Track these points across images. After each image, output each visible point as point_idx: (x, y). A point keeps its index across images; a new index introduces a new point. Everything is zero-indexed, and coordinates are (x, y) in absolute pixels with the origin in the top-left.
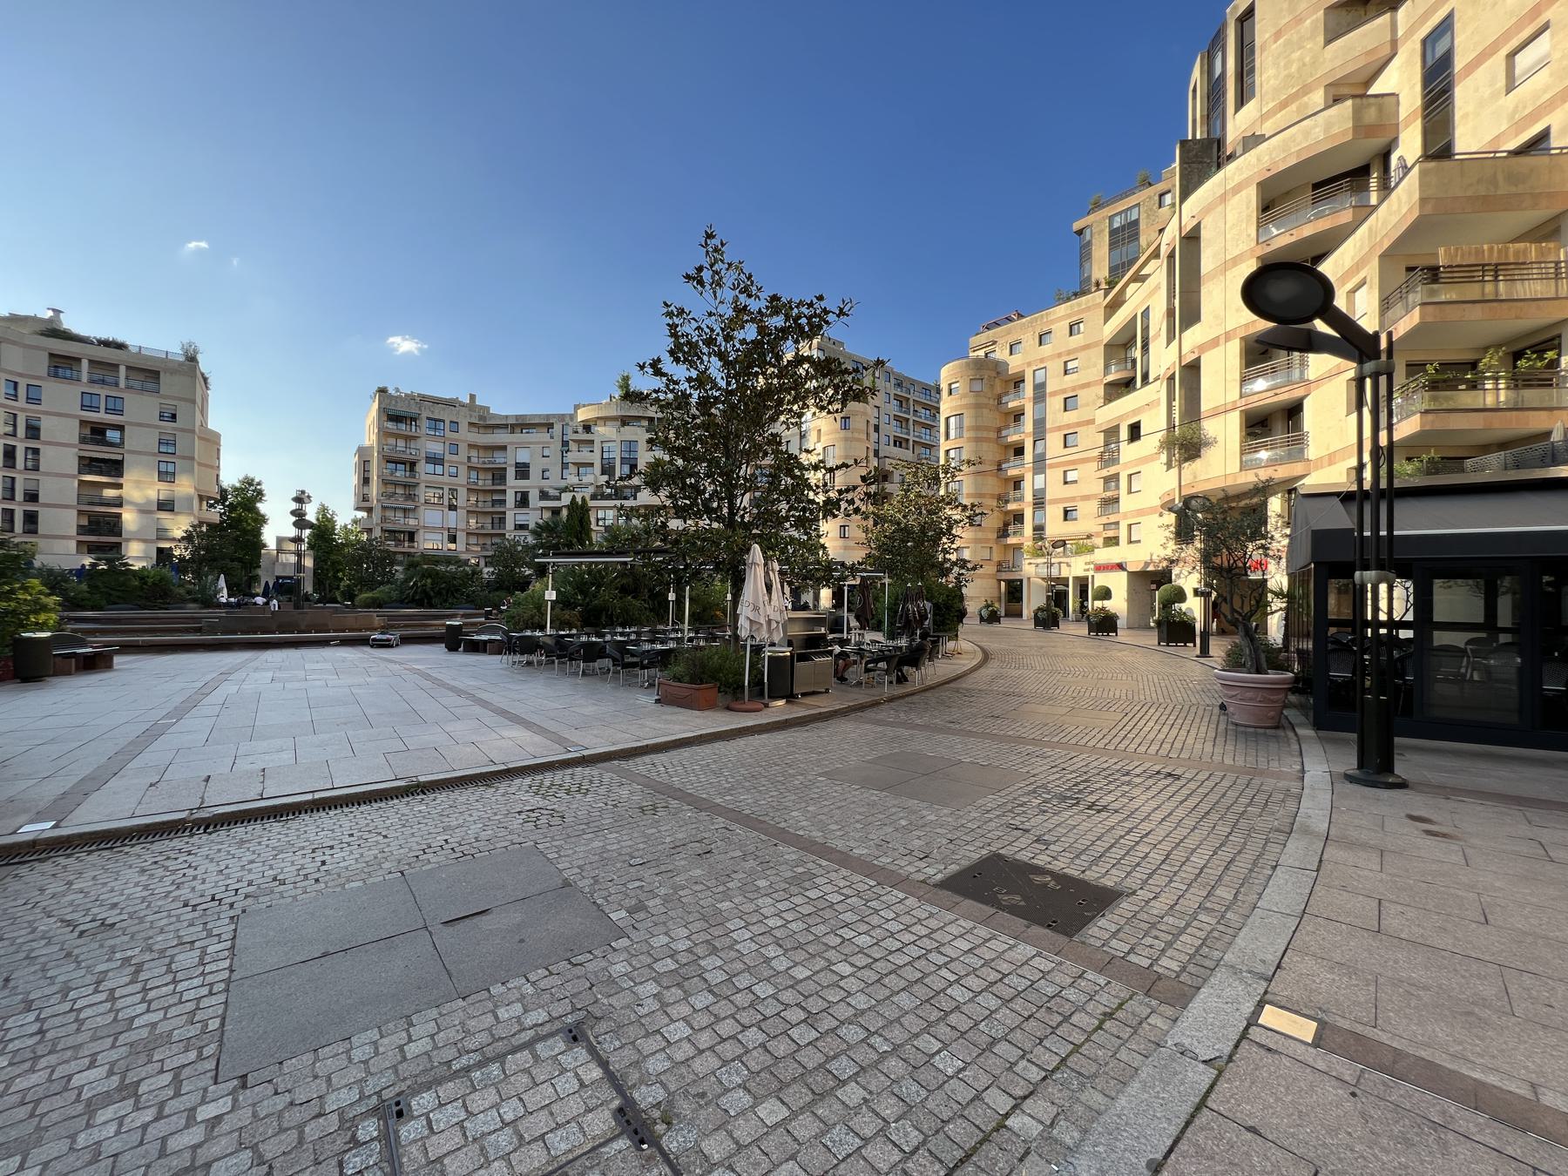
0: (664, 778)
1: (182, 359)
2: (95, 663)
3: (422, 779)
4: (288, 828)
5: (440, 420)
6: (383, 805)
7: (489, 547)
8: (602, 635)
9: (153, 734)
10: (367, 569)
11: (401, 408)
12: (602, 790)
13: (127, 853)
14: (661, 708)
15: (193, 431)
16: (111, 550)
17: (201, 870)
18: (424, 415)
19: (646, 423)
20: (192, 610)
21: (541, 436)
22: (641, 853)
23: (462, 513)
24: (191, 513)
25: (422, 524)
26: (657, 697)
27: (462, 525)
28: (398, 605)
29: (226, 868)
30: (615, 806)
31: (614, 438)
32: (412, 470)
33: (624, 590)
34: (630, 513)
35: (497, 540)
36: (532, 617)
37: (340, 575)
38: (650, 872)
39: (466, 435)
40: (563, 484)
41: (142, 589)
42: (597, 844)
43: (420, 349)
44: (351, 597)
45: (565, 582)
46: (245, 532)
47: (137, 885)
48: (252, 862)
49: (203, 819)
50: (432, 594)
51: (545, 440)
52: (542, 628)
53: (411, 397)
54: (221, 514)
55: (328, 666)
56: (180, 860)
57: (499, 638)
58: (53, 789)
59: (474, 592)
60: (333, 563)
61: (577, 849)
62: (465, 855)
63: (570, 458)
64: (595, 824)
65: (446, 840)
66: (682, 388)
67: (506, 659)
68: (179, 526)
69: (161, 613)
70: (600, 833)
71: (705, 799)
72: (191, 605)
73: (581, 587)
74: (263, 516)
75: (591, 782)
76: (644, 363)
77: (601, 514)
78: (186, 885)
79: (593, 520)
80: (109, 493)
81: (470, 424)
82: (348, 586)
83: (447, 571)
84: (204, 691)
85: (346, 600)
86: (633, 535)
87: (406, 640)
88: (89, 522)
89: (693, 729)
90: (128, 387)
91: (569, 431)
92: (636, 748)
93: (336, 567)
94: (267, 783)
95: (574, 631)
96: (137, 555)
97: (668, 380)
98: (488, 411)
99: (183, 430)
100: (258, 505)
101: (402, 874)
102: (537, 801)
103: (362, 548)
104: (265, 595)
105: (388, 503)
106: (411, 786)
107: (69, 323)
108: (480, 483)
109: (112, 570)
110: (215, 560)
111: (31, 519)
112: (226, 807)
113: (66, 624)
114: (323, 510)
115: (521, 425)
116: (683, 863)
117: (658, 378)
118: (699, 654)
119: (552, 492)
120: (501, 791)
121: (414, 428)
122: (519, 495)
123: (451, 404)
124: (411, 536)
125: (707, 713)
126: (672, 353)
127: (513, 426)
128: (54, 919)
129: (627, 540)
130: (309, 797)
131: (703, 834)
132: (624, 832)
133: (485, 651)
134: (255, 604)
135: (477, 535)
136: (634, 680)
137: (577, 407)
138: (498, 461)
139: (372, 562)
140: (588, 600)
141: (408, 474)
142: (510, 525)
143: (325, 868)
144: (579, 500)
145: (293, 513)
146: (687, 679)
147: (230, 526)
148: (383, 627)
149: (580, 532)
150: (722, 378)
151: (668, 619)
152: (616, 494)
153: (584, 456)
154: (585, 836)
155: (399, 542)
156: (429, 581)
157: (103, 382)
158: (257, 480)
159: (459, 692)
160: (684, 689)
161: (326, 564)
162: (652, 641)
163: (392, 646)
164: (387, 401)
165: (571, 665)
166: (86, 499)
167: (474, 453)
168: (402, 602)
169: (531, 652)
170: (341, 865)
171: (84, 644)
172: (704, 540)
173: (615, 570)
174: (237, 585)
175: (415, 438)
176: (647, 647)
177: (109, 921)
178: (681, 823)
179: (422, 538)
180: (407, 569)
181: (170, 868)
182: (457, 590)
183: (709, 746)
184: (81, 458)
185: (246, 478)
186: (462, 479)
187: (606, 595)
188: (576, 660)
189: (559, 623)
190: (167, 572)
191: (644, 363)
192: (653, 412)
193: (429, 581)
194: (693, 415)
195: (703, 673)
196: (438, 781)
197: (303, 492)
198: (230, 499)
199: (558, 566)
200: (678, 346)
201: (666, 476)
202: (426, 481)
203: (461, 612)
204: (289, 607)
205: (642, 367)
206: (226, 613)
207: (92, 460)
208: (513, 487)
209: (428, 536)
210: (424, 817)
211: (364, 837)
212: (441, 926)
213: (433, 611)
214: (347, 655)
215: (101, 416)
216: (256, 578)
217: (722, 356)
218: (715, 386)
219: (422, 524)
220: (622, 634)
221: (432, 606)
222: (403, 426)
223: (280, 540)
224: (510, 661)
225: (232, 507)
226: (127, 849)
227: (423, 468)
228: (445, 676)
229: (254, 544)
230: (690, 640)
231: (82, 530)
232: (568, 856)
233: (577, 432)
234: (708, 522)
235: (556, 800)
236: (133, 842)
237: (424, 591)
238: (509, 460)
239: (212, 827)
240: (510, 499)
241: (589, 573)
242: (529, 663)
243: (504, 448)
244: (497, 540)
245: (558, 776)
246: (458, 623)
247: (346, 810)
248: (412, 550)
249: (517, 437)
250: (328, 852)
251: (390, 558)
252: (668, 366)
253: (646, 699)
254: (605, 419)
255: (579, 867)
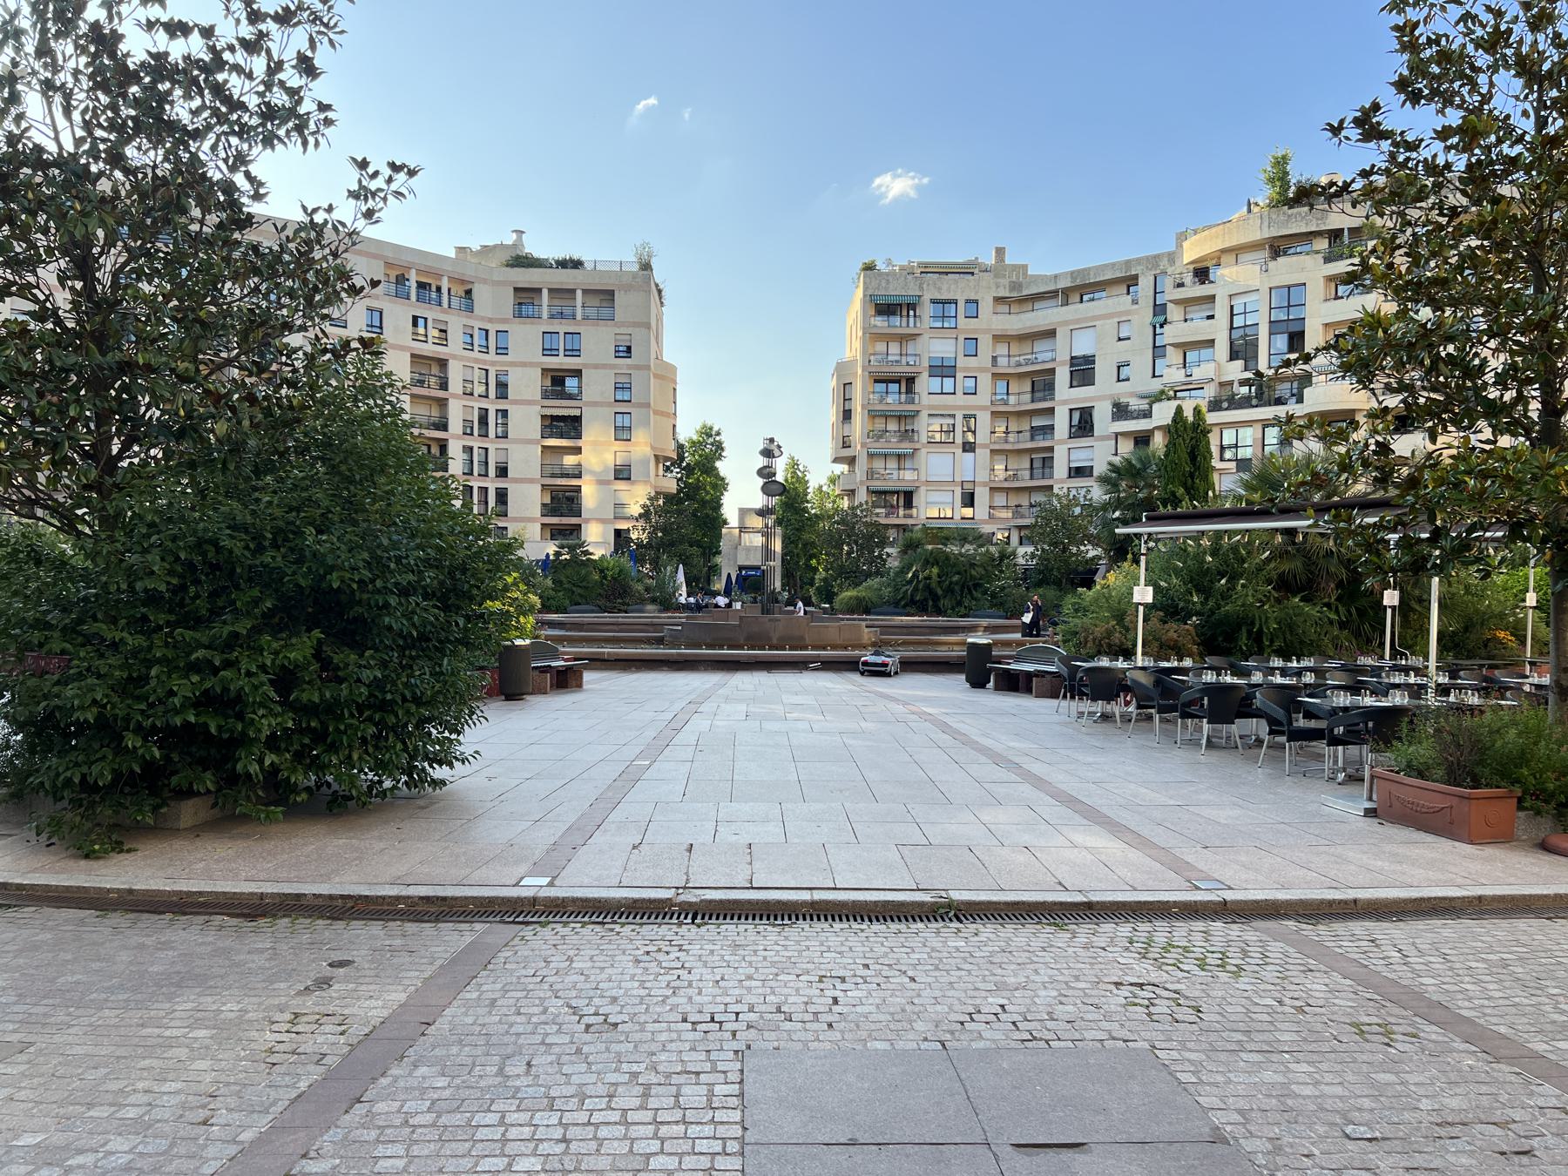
0: (1403, 975)
1: (635, 268)
2: (566, 680)
3: (957, 896)
4: (786, 938)
5: (949, 302)
6: (902, 926)
7: (1024, 511)
8: (1245, 673)
9: (629, 778)
10: (849, 553)
11: (896, 291)
12: (1270, 973)
13: (618, 933)
14: (1380, 829)
15: (648, 367)
16: (571, 534)
17: (694, 977)
18: (927, 297)
19: (1322, 244)
20: (651, 612)
21: (1113, 302)
22: (1367, 1116)
23: (983, 454)
24: (646, 482)
25: (923, 478)
26: (1368, 805)
27: (982, 476)
28: (891, 609)
29: (722, 979)
30: (1300, 1010)
31: (1255, 284)
32: (910, 390)
33: (1286, 585)
34: (1291, 430)
35: (1039, 498)
36: (1109, 633)
37: (814, 562)
38: (1391, 1160)
39: (992, 320)
40: (1155, 386)
41: (603, 584)
42: (1268, 1076)
43: (918, 188)
44: (829, 596)
45: (1168, 570)
46: (704, 503)
47: (633, 977)
48: (750, 978)
49: (690, 904)
50: (940, 592)
51: (1122, 309)
52: (1128, 654)
53: (908, 271)
54: (679, 480)
55: (808, 700)
56: (672, 956)
57: (1053, 669)
58: (545, 836)
59: (1003, 588)
60: (805, 545)
61: (1231, 1075)
62: (1035, 1038)
63: (1170, 334)
64: (1265, 1037)
65: (1002, 1006)
66: (1425, 153)
67: (1067, 707)
68: (636, 498)
69: (620, 617)
70: (1275, 1057)
71: (1503, 1037)
72: (650, 607)
73: (1200, 579)
74: (723, 479)
75: (1245, 953)
76: (1342, 122)
77: (1229, 437)
78: (682, 992)
79: (1215, 450)
80: (569, 460)
81: (999, 300)
82: (825, 580)
83: (961, 554)
84: (673, 725)
85: (822, 601)
86: (1315, 475)
87: (910, 666)
88: (552, 498)
89: (1460, 881)
90: (585, 318)
91: (1167, 284)
92: (1331, 903)
93: (809, 550)
94: (756, 865)
95: (1188, 663)
96: (597, 540)
97: (1396, 144)
98: (1025, 274)
99: (637, 367)
100: (718, 464)
101: (944, 1045)
102: (1144, 971)
103: (843, 522)
104: (727, 593)
105: (879, 446)
106: (942, 906)
107: (535, 247)
108: (1012, 399)
109: (573, 559)
110: (672, 544)
111: (502, 496)
112: (713, 892)
113: (541, 628)
114: (794, 465)
115: (1083, 289)
116: (1464, 1160)
117: (1372, 145)
118: (1467, 721)
119: (1136, 404)
120: (1082, 939)
121: (911, 320)
122: (1076, 416)
123: (966, 270)
124: (908, 497)
125: (1489, 851)
126: (1402, 85)
127: (1066, 292)
128: (560, 1002)
129: (1303, 483)
130: (805, 896)
131: (1509, 1111)
132: (1324, 1066)
133: (1028, 690)
134: (717, 606)
135: (1008, 490)
136: (1315, 766)
137: (1182, 237)
138: (1041, 357)
139: (856, 543)
140: (1211, 603)
141: (903, 397)
142: (1060, 469)
143: (836, 1009)
144: (1189, 414)
145: (760, 472)
146: (1440, 772)
147: (688, 497)
148: (874, 644)
149: (1192, 476)
150: (1525, 114)
151: (1382, 644)
152: (1259, 395)
153: (1198, 328)
154: (1244, 1056)
155: (892, 509)
156: (935, 570)
157: (561, 315)
158: (716, 429)
159: (998, 759)
160: (1432, 794)
161: (797, 547)
162: (1355, 689)
163: (888, 675)
164: (874, 283)
165: (1185, 727)
166: (549, 470)
167: (1002, 349)
168: (896, 604)
169: (1110, 697)
170: (859, 1009)
171: (555, 655)
172: (1484, 475)
173: (1264, 546)
174: (697, 580)
175: (913, 337)
176: (1343, 700)
177: (612, 1019)
178: (1453, 1076)
179: (923, 499)
180: (904, 552)
181: (664, 964)
182: (977, 586)
183: (1504, 923)
184: (543, 417)
185: (704, 426)
186: (984, 398)
187: (1247, 595)
188: (1193, 716)
189: (1159, 647)
190: (626, 562)
191: (1342, 122)
192: (1342, 217)
193: (935, 570)
194: (1453, 209)
195: (1481, 762)
196: (980, 903)
197: (772, 440)
198: (688, 458)
199: (1157, 541)
200: (1418, 68)
201: (1391, 345)
202: (930, 407)
203: (985, 622)
204: (756, 611)
205: (1336, 130)
206: (687, 618)
207: (554, 418)
208: (1065, 402)
209: (935, 497)
210: (964, 959)
211: (884, 973)
212: (1010, 1149)
213: (941, 620)
214: (829, 685)
215: (561, 361)
216: (714, 570)
217: (1527, 68)
218: (1506, 130)
219: (923, 478)
220: (1284, 672)
221: (939, 612)
222: (896, 320)
223: (743, 512)
224: (1074, 713)
225: (689, 470)
226: (617, 928)
227: (925, 384)
228: (970, 728)
229: (713, 522)
230: (1443, 690)
231: (547, 510)
232: (1216, 1085)
233: (1181, 285)
234: (1487, 433)
235: (1181, 974)
236: (623, 920)
237: (928, 588)
238: (1059, 354)
239: (699, 917)
240: (1061, 423)
241: (1215, 552)
242: (1106, 717)
243: (1051, 334)
244: (1039, 498)
245: (1182, 931)
246: (985, 641)
247: (855, 925)
248: (910, 522)
249: (1076, 310)
250: (839, 986)
251: (875, 537)
252: (1399, 117)
253: (1348, 807)
254: (1237, 251)
255: (1240, 1112)
